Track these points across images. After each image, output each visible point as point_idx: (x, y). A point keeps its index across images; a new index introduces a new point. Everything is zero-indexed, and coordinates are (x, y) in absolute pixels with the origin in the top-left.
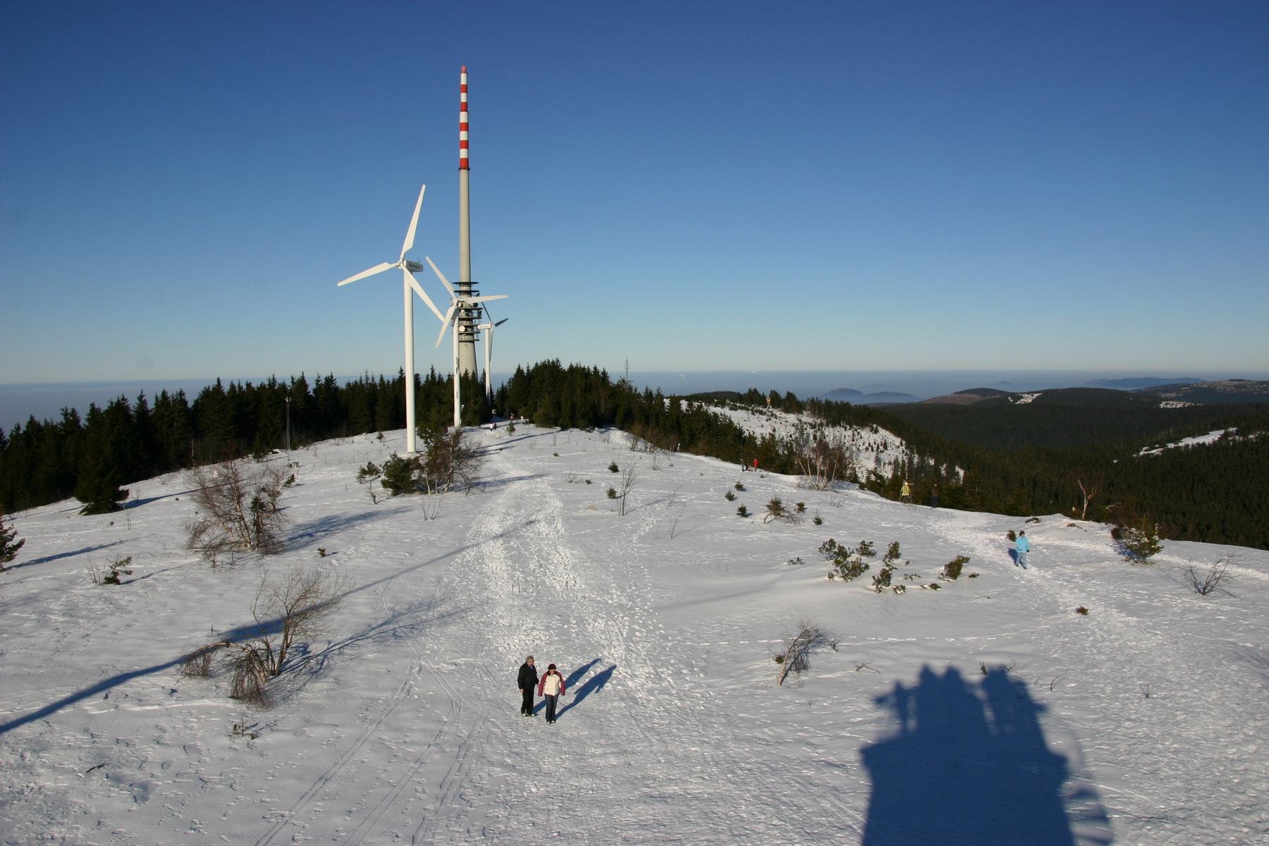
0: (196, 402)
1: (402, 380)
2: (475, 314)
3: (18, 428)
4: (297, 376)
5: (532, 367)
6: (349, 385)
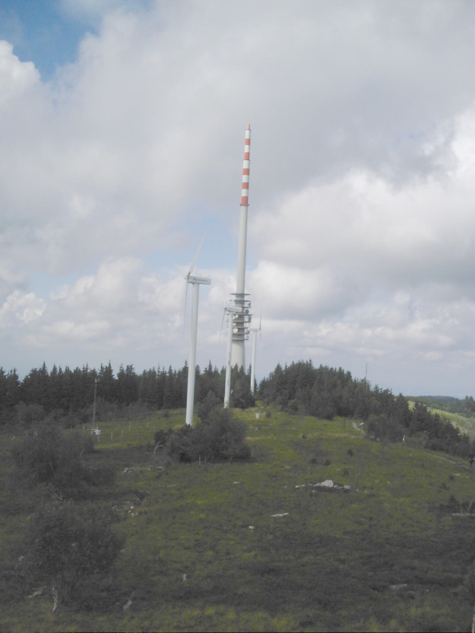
0: (26, 380)
1: (186, 370)
2: (246, 319)
3: (206, 369)
4: (105, 365)
5: (289, 364)
6: (145, 372)
